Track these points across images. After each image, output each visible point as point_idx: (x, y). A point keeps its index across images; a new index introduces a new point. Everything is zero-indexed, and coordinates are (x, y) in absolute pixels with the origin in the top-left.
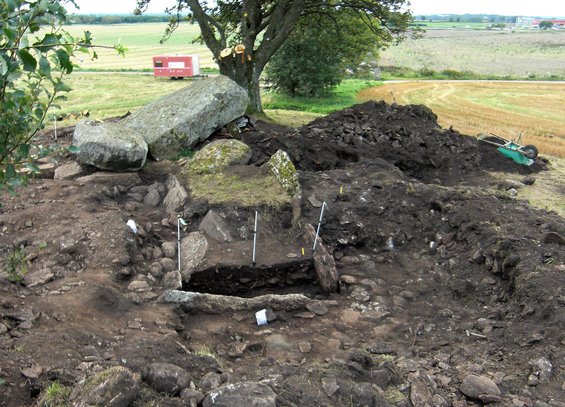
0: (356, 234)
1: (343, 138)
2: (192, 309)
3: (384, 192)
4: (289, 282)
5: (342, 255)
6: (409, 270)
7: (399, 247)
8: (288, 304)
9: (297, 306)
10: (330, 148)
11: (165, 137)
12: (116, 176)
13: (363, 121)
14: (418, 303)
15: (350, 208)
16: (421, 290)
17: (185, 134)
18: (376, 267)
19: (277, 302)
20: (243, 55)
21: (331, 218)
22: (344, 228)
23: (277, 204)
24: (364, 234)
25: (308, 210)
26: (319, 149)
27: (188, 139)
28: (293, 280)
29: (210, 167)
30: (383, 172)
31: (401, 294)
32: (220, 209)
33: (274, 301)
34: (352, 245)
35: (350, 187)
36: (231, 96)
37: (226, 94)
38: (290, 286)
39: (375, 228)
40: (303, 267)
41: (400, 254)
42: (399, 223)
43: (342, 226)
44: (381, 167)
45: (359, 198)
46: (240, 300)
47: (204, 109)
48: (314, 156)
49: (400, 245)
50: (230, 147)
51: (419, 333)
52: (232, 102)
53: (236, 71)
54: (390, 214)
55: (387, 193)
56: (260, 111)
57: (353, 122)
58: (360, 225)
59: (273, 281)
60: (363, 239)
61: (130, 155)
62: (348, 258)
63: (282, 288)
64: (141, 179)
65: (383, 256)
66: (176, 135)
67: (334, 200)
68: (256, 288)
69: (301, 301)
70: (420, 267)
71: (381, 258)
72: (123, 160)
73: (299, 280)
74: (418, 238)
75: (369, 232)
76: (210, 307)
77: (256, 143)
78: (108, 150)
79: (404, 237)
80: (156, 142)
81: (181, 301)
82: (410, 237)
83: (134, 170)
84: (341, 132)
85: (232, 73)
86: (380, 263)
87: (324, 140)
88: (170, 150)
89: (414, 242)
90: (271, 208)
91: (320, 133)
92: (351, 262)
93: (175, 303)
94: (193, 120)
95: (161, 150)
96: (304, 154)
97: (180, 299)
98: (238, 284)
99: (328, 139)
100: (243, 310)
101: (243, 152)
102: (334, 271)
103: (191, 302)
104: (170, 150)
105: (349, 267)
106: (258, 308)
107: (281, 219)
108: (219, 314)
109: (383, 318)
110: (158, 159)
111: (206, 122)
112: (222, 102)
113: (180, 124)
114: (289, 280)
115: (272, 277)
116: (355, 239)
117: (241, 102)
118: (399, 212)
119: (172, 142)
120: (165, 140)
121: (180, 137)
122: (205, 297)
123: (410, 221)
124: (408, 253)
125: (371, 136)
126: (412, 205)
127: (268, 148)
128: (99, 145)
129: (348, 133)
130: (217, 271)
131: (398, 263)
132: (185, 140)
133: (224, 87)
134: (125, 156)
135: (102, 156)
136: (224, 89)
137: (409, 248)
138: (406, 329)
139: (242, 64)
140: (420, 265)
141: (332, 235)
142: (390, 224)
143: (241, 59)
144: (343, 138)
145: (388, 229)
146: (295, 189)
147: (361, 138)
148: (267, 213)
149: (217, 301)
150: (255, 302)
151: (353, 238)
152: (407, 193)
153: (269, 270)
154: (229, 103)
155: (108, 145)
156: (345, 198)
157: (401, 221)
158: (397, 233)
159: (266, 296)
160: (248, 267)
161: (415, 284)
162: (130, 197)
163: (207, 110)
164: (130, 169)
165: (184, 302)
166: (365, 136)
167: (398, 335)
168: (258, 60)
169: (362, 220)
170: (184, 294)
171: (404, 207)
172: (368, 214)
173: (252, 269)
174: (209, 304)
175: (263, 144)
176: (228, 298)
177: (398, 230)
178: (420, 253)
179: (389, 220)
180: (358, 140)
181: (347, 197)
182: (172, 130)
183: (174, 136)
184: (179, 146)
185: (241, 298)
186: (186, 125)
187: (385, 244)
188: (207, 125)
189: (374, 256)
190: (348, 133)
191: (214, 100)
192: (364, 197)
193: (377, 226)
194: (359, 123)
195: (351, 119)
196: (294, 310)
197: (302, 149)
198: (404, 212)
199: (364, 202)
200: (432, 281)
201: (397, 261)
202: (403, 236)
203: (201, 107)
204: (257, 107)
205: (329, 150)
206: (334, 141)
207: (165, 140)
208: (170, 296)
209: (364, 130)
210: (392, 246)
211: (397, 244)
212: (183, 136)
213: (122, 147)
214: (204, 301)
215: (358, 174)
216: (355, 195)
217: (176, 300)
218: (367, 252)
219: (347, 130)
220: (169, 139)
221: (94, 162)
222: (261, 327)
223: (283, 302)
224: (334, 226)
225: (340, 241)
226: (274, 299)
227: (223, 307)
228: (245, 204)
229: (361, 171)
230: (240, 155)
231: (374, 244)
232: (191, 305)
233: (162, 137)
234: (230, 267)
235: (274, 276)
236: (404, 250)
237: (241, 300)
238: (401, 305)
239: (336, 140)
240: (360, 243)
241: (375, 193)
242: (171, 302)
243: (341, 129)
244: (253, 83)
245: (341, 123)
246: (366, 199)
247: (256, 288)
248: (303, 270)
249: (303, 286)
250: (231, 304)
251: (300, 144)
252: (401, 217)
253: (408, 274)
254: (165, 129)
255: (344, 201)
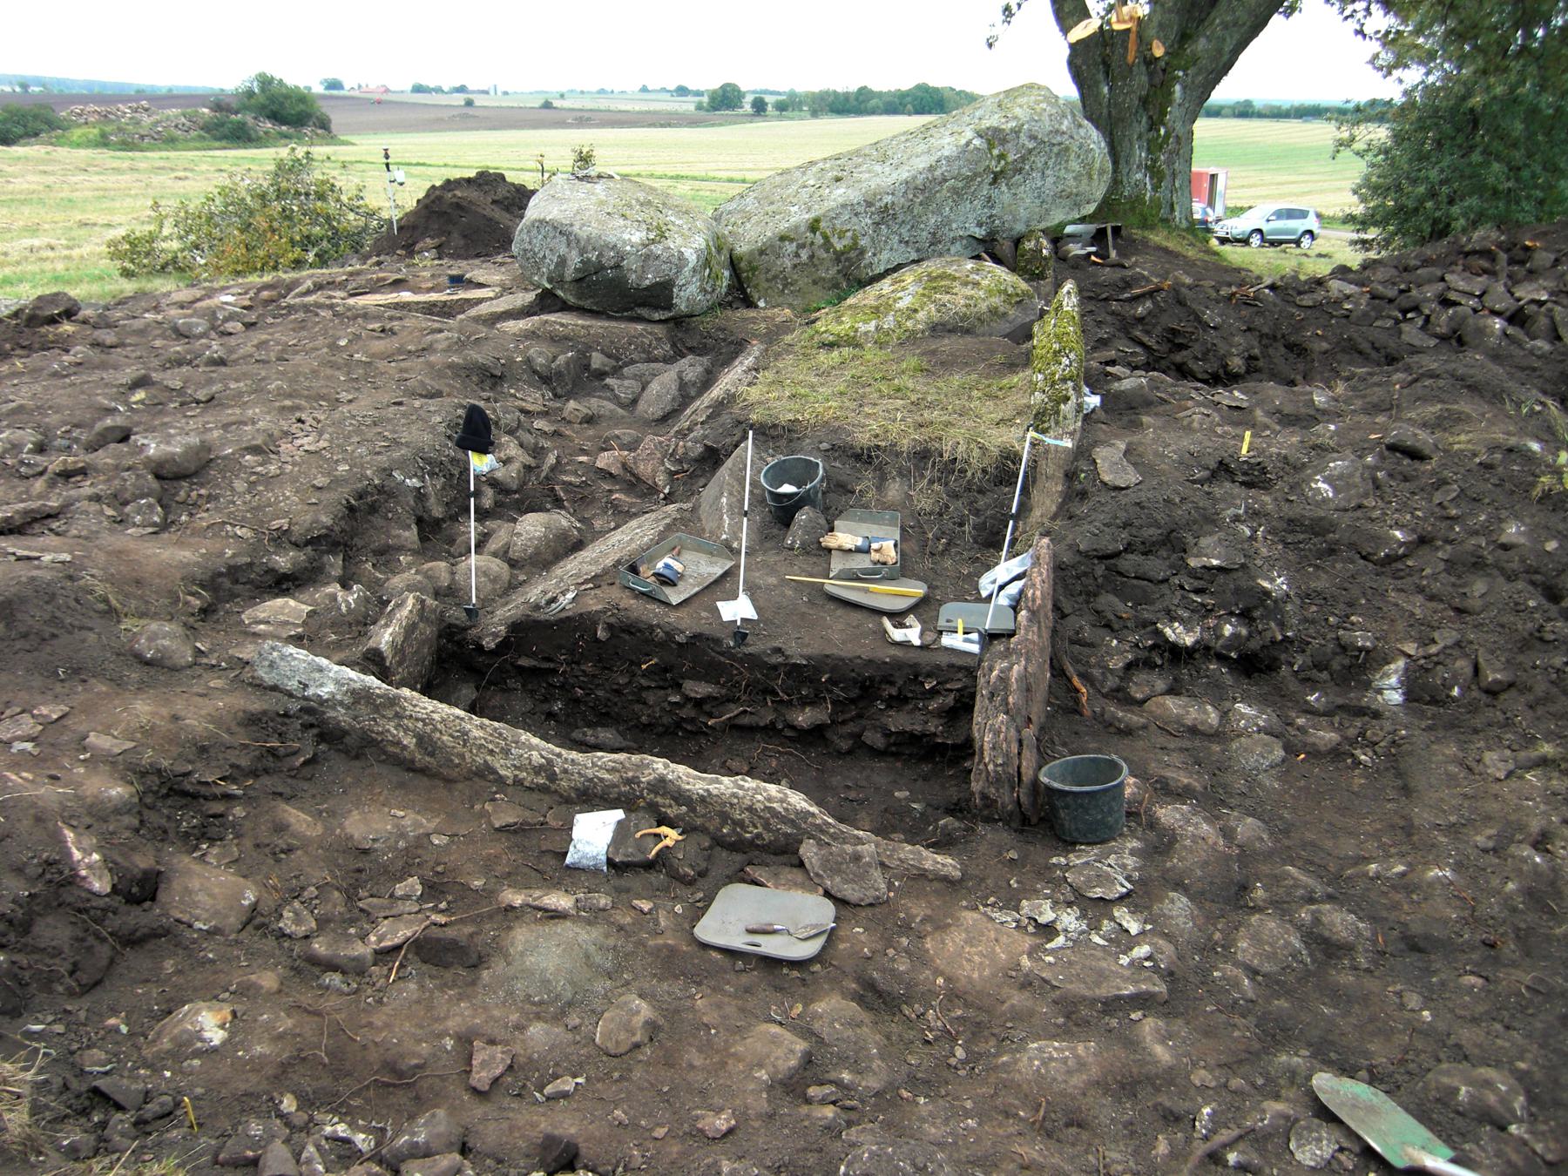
0: (1246, 616)
1: (1427, 319)
2: (345, 733)
3: (1433, 473)
4: (874, 738)
5: (1161, 685)
6: (1422, 815)
7: (1431, 710)
8: (725, 817)
9: (768, 837)
10: (1365, 346)
11: (792, 240)
12: (598, 325)
13: (1531, 272)
14: (1371, 984)
15: (1254, 515)
16: (1416, 928)
17: (855, 239)
18: (1284, 769)
19: (681, 797)
20: (1133, 36)
21: (1151, 533)
22: (1198, 584)
23: (976, 453)
24: (1282, 625)
25: (1083, 495)
26: (1325, 345)
27: (862, 252)
28: (888, 734)
29: (863, 328)
30: (1465, 406)
31: (1304, 915)
32: (783, 442)
33: (660, 785)
34: (1222, 658)
35: (1295, 439)
36: (1033, 137)
37: (1016, 132)
38: (876, 753)
39: (1341, 608)
40: (934, 692)
41: (1421, 738)
42: (1459, 611)
43: (1193, 574)
44: (1469, 387)
45: (1310, 479)
46: (531, 748)
47: (931, 169)
48: (1301, 367)
49: (1434, 701)
50: (955, 279)
51: (1232, 1158)
52: (1040, 162)
53: (1111, 89)
54: (1431, 564)
55: (1442, 483)
56: (1184, 224)
57: (1485, 271)
58: (1278, 584)
59: (804, 718)
60: (1273, 642)
61: (631, 264)
62: (1172, 705)
63: (841, 754)
64: (674, 345)
65: (1340, 729)
66: (826, 238)
67: (1199, 474)
68: (737, 729)
69: (784, 819)
70: (1488, 818)
71: (1326, 736)
72: (612, 280)
73: (913, 738)
74: (1541, 687)
75: (1306, 620)
76: (411, 741)
77: (1106, 299)
78: (573, 244)
79: (1469, 671)
80: (762, 252)
81: (310, 692)
82: (1492, 676)
83: (656, 316)
84: (1428, 300)
85: (1099, 93)
86: (1315, 754)
87: (1354, 316)
88: (803, 282)
89: (1515, 703)
90: (950, 467)
91: (1348, 297)
92: (1178, 720)
93: (290, 695)
94: (888, 199)
95: (775, 277)
96: (1266, 355)
97: (306, 686)
98: (675, 699)
99: (1365, 314)
100: (543, 789)
101: (996, 301)
102: (997, 733)
103: (341, 703)
104: (803, 282)
105: (1162, 740)
106: (592, 797)
107: (977, 513)
108: (449, 781)
109: (1113, 1005)
110: (761, 304)
111: (938, 212)
112: (1001, 157)
113: (844, 206)
114: (875, 727)
115: (804, 702)
116: (1235, 636)
117: (1075, 165)
118: (1478, 565)
119: (812, 257)
120: (790, 248)
121: (839, 247)
122: (393, 701)
123: (1519, 609)
124: (1462, 745)
125: (1543, 321)
126: (1551, 546)
127: (1140, 320)
128: (555, 228)
129: (1455, 304)
130: (601, 634)
131: (1399, 775)
132: (853, 254)
133: (1018, 111)
134: (617, 266)
135: (562, 262)
136: (1015, 118)
137: (1478, 722)
138: (1181, 1106)
139: (1130, 68)
140: (1493, 807)
141: (1142, 600)
142: (1418, 606)
143: (1126, 49)
144: (1427, 319)
145: (1401, 625)
146: (1057, 412)
147: (1498, 324)
148: (931, 482)
149: (435, 729)
150: (589, 773)
151: (1228, 630)
152: (1537, 492)
153: (794, 670)
154: (1023, 159)
155: (576, 229)
156: (1255, 477)
157: (1475, 603)
158: (1433, 649)
159: (635, 758)
160: (718, 641)
161: (1405, 885)
162: (607, 387)
163: (938, 173)
164: (644, 312)
165: (322, 701)
166: (1517, 318)
167: (1129, 1124)
168: (1195, 60)
169: (1295, 572)
170: (320, 670)
171: (1506, 547)
172: (1332, 551)
173: (727, 653)
174: (406, 730)
175: (1127, 306)
176: (482, 727)
177: (1445, 637)
178: (1522, 755)
179: (1421, 590)
180: (1481, 331)
181: (1264, 471)
182: (817, 220)
183: (819, 240)
184: (833, 272)
185: (535, 741)
186: (860, 209)
187: (1367, 685)
188: (947, 223)
189: (1300, 721)
190: (1455, 304)
191: (968, 143)
192: (1326, 480)
193: (1350, 605)
194: (1510, 277)
195: (1485, 264)
196: (751, 844)
197: (1262, 336)
198: (1502, 571)
199: (1325, 500)
200: (1509, 897)
201: (1395, 760)
202: (1463, 665)
203: (922, 163)
204: (1172, 209)
205: (1360, 353)
206: (1389, 323)
207: (790, 248)
208: (272, 665)
209: (1519, 300)
210: (1396, 697)
211: (1419, 692)
212: (846, 242)
213: (612, 239)
214: (390, 714)
215: (1359, 403)
216: (1298, 468)
217: (292, 685)
218: (1277, 698)
219: (1453, 296)
220: (802, 246)
221: (550, 280)
222: (573, 876)
223: (703, 799)
224: (1156, 566)
225: (1168, 631)
226: (662, 780)
227: (462, 756)
228: (863, 439)
229: (1377, 394)
230: (983, 306)
231: (1315, 674)
232: (340, 715)
233: (782, 238)
234: (651, 628)
235: (814, 701)
236: (1452, 725)
237: (535, 747)
238: (1267, 967)
239: (1397, 322)
240: (1255, 655)
241: (1391, 475)
242: (275, 688)
243: (1430, 292)
244: (1167, 135)
245: (1439, 273)
246: (1336, 490)
247: (737, 729)
248: (933, 705)
249: (926, 768)
250: (491, 752)
251: (1259, 321)
252: (1479, 587)
253: (1408, 829)
254: (798, 216)
255: (1248, 485)
